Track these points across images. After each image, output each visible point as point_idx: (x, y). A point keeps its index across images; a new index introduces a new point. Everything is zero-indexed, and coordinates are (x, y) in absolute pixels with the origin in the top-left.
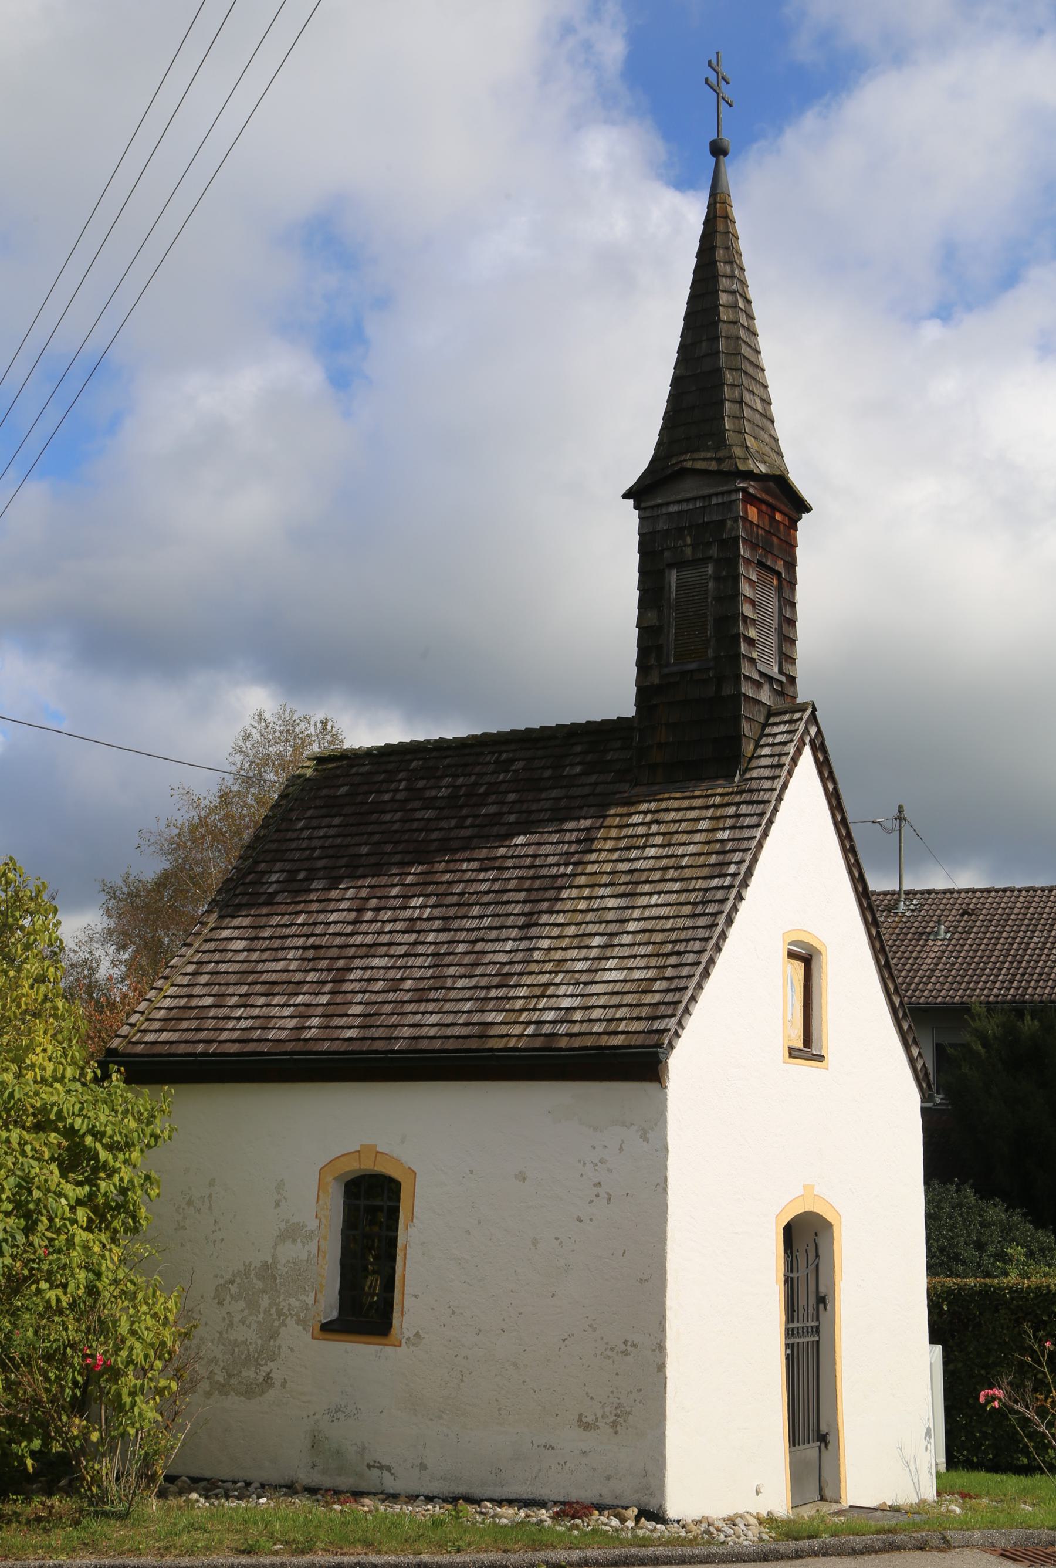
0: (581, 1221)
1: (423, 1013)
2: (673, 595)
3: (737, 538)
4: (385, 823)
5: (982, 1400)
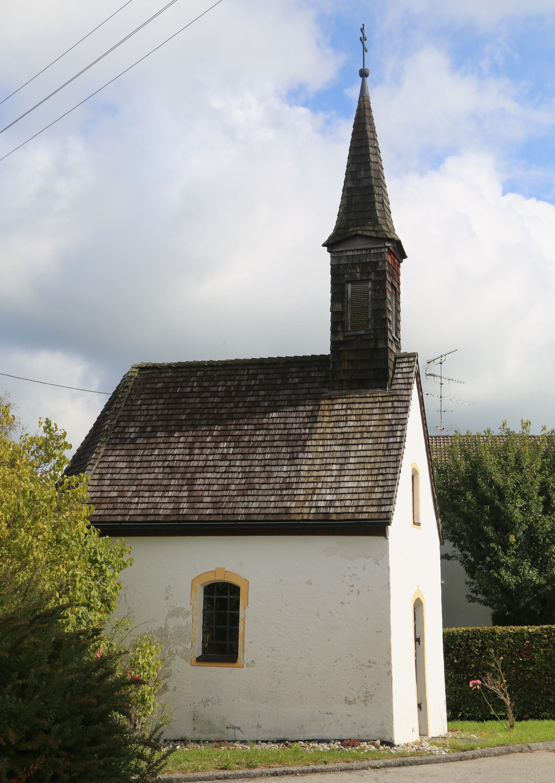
0: (343, 604)
1: (248, 502)
2: (349, 297)
3: (385, 271)
4: (191, 403)
5: (471, 685)
